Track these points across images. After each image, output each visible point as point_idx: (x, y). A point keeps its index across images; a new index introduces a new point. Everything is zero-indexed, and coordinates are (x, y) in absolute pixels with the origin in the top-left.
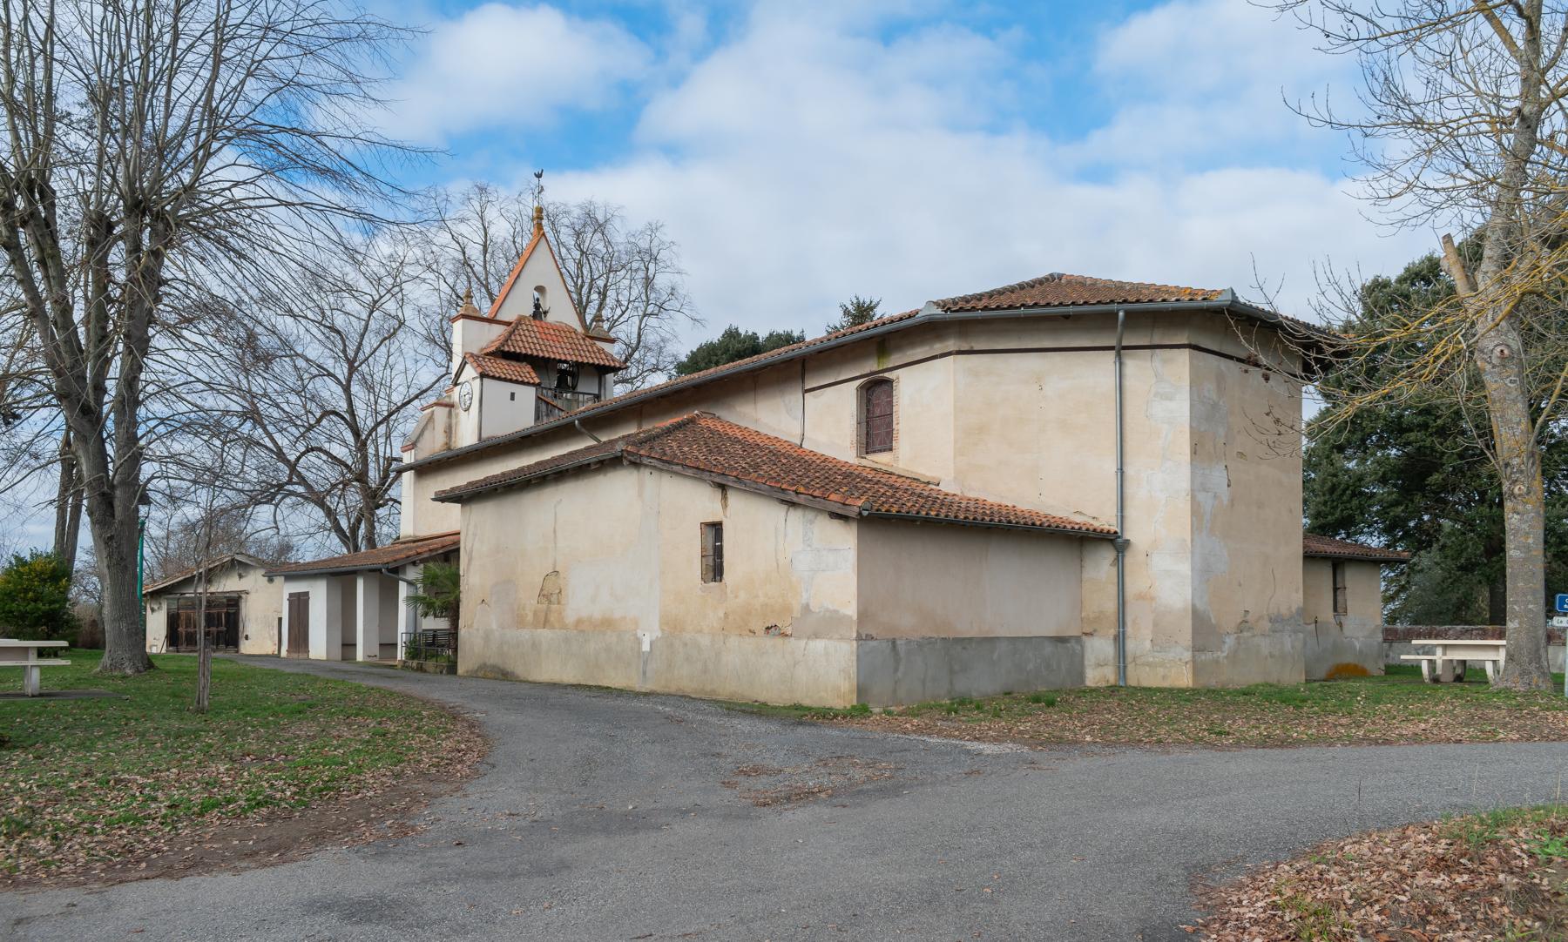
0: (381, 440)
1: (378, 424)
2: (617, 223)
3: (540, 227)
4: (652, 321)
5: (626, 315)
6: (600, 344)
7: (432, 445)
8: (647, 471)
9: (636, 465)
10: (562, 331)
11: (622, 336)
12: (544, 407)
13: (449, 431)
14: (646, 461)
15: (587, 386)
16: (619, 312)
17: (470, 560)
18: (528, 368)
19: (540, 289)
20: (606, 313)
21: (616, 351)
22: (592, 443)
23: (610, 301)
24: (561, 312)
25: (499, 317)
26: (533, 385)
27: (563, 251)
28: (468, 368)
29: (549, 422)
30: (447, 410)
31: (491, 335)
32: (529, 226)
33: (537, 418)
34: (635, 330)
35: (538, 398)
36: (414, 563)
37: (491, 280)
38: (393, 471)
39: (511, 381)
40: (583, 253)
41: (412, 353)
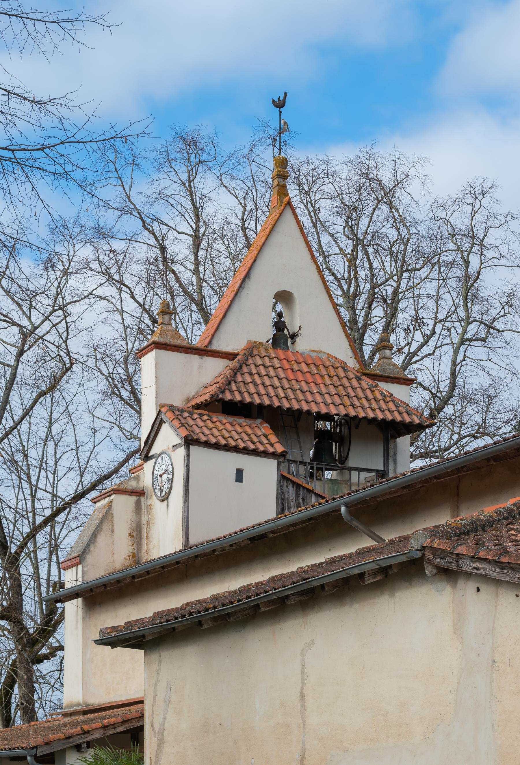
0: (43, 554)
1: (36, 529)
2: (414, 188)
3: (282, 191)
4: (476, 351)
5: (432, 342)
6: (384, 386)
7: (111, 557)
8: (470, 586)
9: (449, 574)
10: (323, 366)
11: (424, 378)
12: (291, 493)
13: (137, 534)
14: (468, 566)
15: (365, 458)
16: (419, 337)
17: (161, 744)
18: (264, 429)
19: (284, 297)
20: (397, 339)
21: (415, 399)
22: (369, 543)
23: (403, 318)
24: (320, 334)
25: (216, 346)
26: (274, 455)
27: (325, 239)
28: (166, 429)
29: (294, 515)
30: (133, 499)
31: (203, 376)
32: (266, 196)
33: (281, 508)
34: (446, 368)
35: (282, 478)
36: (78, 748)
37: (207, 291)
38: (56, 598)
39: (236, 449)
40: (357, 242)
41: (87, 417)
